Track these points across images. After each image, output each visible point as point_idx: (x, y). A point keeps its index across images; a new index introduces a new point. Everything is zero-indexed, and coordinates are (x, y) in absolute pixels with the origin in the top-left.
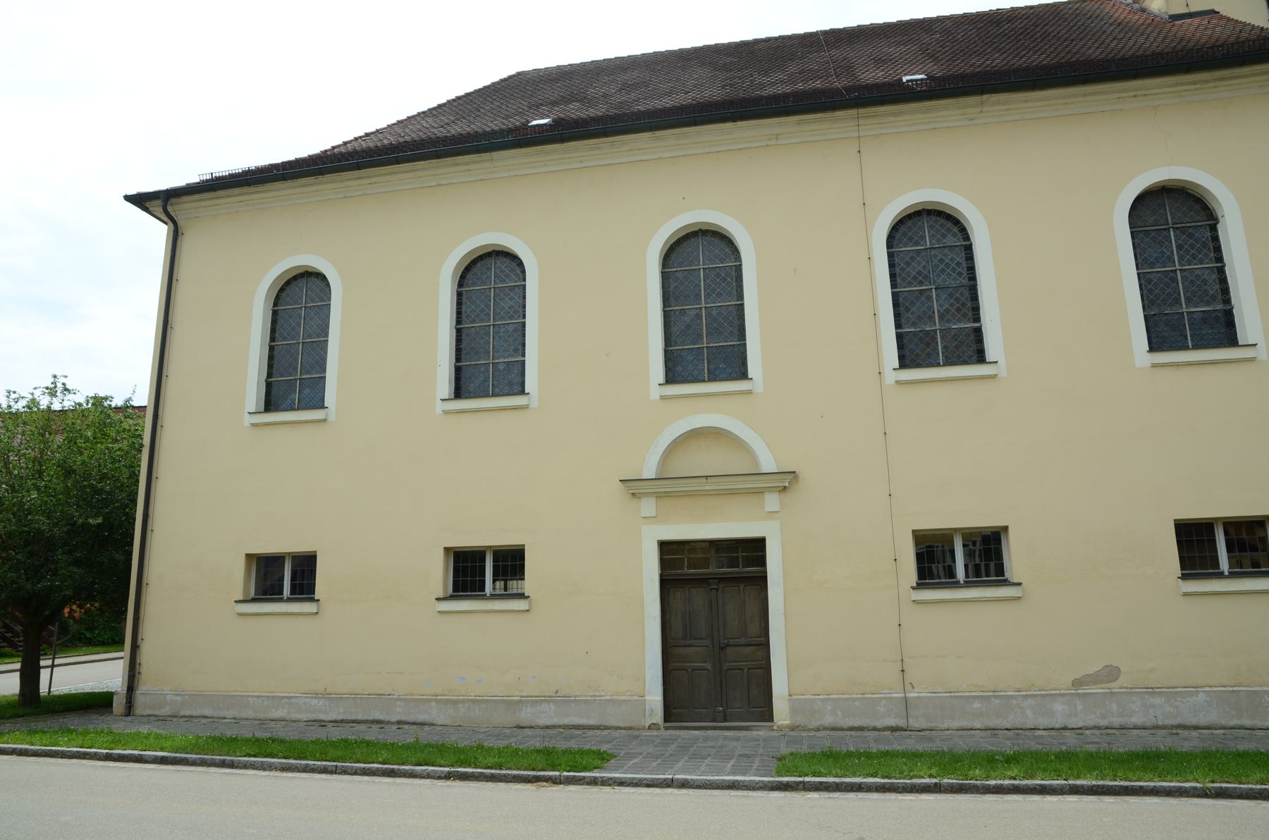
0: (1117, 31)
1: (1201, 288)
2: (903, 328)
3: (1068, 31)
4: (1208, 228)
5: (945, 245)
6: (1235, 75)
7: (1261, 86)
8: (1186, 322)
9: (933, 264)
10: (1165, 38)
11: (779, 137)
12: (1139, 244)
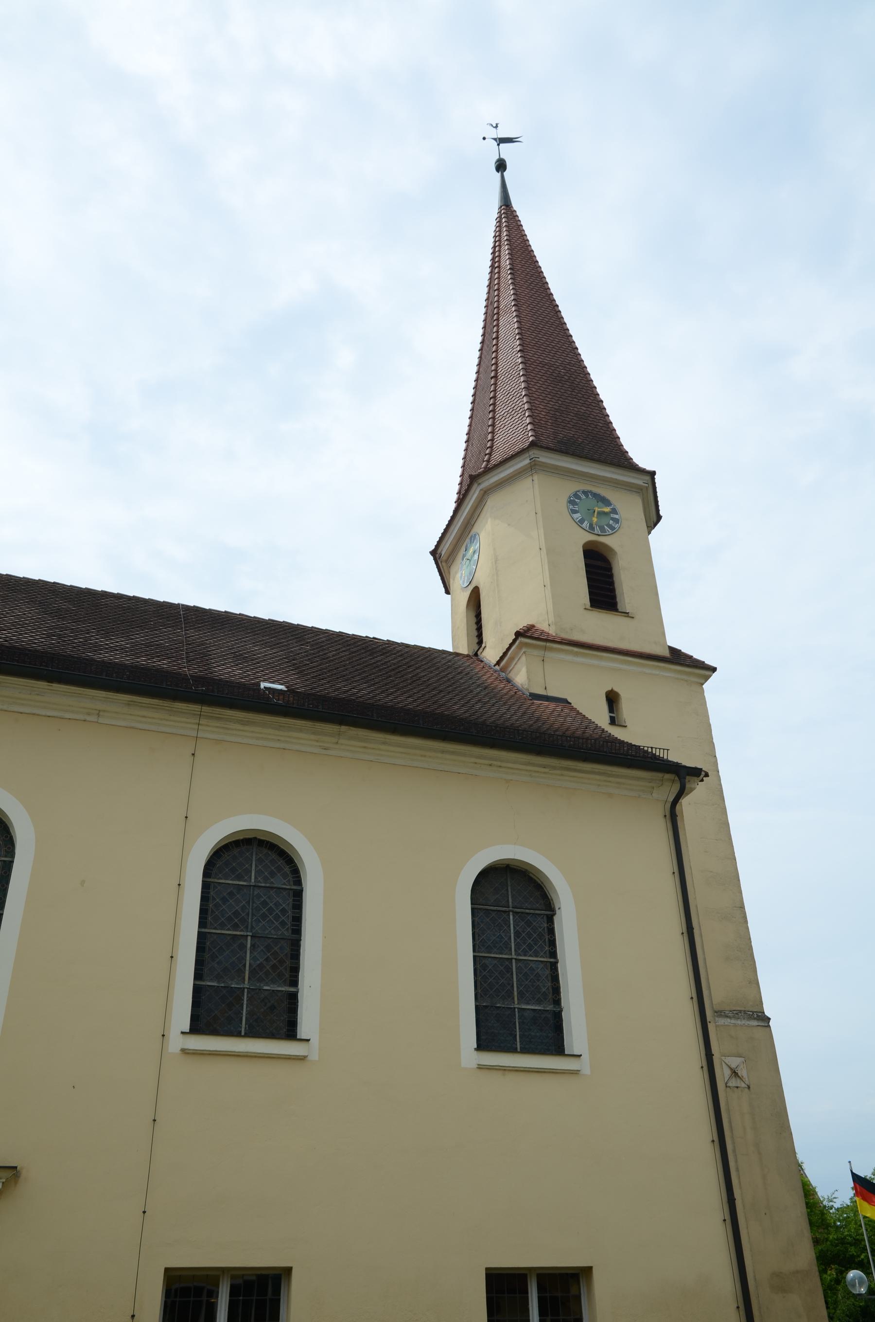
0: (483, 693)
1: (534, 984)
2: (204, 981)
3: (438, 680)
4: (545, 917)
5: (272, 885)
6: (578, 768)
7: (599, 785)
8: (517, 1020)
9: (255, 905)
10: (524, 713)
11: (101, 713)
12: (478, 923)
